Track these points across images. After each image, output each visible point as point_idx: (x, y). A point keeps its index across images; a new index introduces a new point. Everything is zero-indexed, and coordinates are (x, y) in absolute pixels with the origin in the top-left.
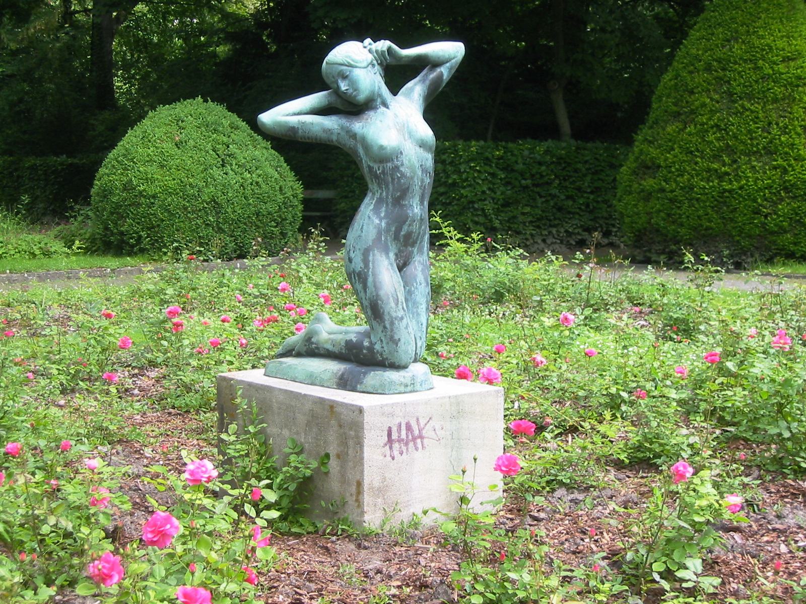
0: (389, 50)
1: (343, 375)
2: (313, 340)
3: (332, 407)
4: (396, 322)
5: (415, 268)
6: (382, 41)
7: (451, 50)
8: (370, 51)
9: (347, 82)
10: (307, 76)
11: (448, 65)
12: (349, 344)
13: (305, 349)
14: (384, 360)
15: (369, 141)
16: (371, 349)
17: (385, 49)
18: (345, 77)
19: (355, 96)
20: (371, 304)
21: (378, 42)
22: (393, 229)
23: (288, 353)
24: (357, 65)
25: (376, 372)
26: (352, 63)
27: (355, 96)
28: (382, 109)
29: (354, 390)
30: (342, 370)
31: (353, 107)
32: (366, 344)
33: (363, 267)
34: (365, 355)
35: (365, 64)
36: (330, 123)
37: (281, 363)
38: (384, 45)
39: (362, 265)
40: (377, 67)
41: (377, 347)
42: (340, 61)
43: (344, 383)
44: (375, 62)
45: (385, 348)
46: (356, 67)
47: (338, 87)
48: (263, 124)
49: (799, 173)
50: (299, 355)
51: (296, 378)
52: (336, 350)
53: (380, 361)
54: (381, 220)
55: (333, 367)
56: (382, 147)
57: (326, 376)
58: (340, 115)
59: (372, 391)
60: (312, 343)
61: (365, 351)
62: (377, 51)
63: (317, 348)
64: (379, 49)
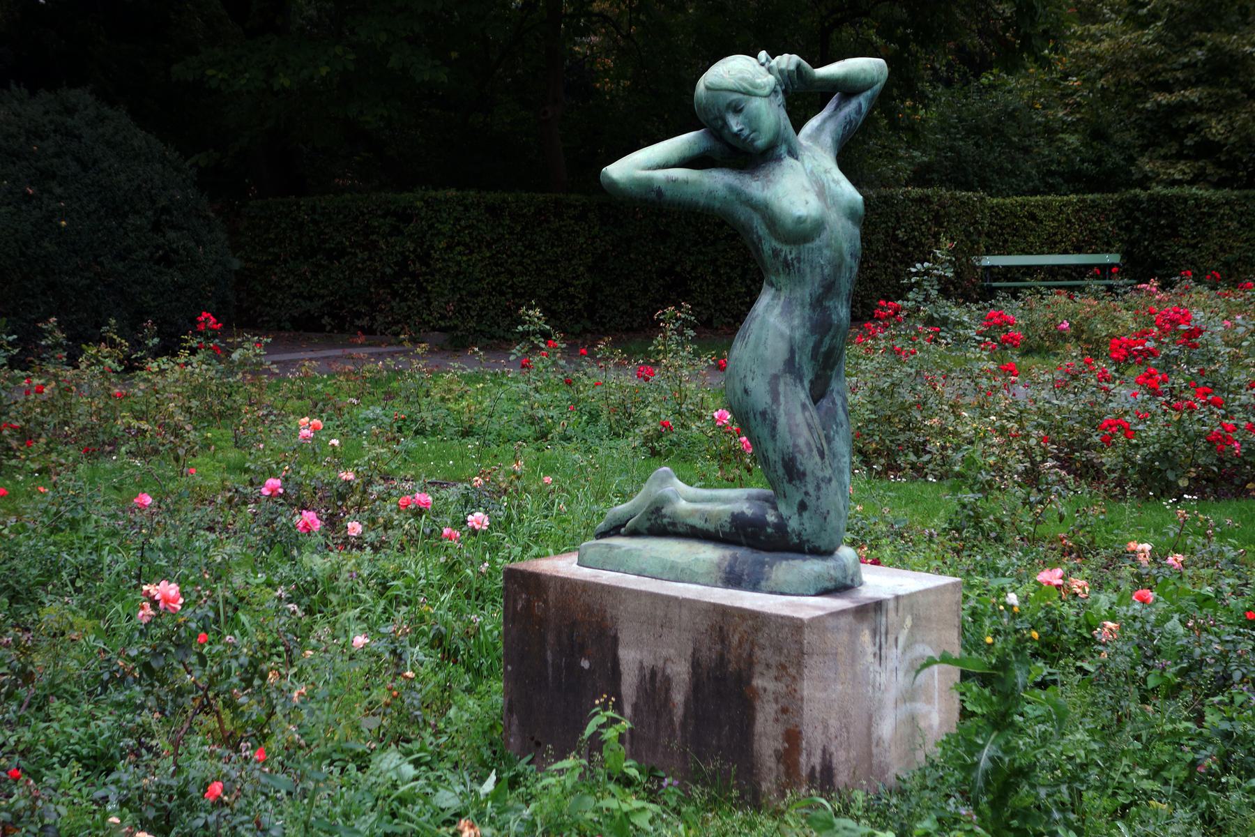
0: (799, 66)
1: (731, 566)
2: (664, 511)
3: (724, 612)
4: (823, 485)
5: (834, 403)
6: (786, 56)
7: (865, 66)
8: (770, 70)
9: (741, 118)
10: (669, 109)
11: (869, 93)
12: (737, 519)
13: (647, 524)
14: (802, 543)
15: (777, 210)
16: (781, 526)
17: (792, 67)
18: (737, 109)
19: (753, 140)
20: (783, 459)
21: (778, 58)
22: (811, 344)
23: (615, 530)
24: (757, 91)
25: (791, 562)
26: (750, 88)
27: (753, 140)
28: (789, 161)
29: (755, 587)
30: (728, 558)
31: (750, 156)
32: (771, 518)
33: (769, 401)
34: (769, 536)
35: (767, 91)
36: (715, 181)
37: (611, 547)
38: (788, 61)
39: (768, 399)
40: (781, 96)
41: (793, 524)
42: (731, 86)
43: (733, 579)
44: (778, 88)
45: (807, 525)
46: (756, 95)
47: (725, 124)
48: (613, 183)
49: (1, 353)
50: (634, 533)
51: (645, 570)
52: (710, 527)
53: (795, 544)
54: (792, 329)
55: (709, 554)
56: (800, 220)
57: (701, 569)
58: (725, 170)
59: (787, 591)
60: (664, 516)
61: (769, 530)
62: (781, 72)
63: (674, 524)
64: (783, 66)
